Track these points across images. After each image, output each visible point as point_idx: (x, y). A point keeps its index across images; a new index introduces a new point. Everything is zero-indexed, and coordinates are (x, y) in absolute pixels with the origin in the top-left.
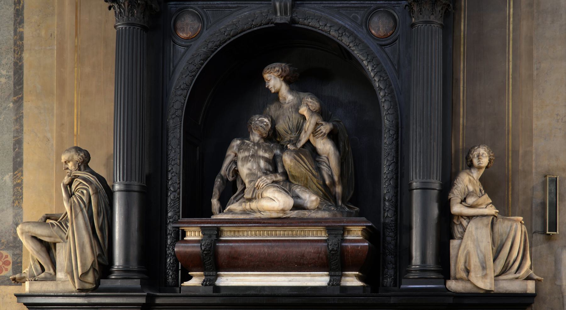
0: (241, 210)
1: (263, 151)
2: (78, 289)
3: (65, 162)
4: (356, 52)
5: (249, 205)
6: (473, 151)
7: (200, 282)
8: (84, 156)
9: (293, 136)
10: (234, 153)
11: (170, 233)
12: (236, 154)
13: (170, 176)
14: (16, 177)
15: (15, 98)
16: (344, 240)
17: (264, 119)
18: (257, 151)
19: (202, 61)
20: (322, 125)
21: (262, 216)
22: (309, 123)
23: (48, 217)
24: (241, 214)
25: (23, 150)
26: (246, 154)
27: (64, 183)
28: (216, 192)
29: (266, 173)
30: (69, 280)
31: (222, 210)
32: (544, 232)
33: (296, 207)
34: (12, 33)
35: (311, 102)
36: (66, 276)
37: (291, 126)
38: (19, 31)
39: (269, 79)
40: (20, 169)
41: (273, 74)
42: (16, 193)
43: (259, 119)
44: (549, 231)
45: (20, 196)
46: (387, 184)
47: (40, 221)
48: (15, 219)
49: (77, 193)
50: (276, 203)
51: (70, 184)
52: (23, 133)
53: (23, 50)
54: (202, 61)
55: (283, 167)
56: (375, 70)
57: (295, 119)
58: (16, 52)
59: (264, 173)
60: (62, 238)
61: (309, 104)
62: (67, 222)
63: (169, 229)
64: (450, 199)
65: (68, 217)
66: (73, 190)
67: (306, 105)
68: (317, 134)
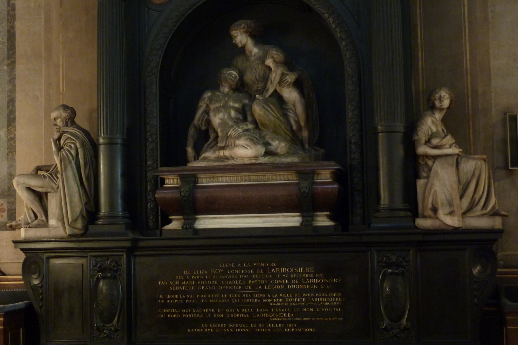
0: (215, 157)
1: (233, 101)
2: (68, 235)
3: (54, 119)
4: (317, 6)
5: (222, 153)
6: (434, 93)
7: (180, 225)
8: (71, 113)
9: (260, 86)
10: (206, 104)
11: (150, 180)
12: (207, 105)
13: (148, 128)
14: (10, 132)
15: (9, 62)
16: (314, 183)
17: (232, 71)
18: (227, 102)
19: (174, 24)
20: (287, 75)
21: (236, 163)
22: (275, 74)
23: (39, 168)
24: (216, 161)
25: (16, 108)
26: (218, 105)
27: (54, 138)
28: (190, 141)
29: (237, 122)
30: (60, 227)
31: (197, 157)
32: (506, 168)
33: (268, 153)
34: (6, 4)
35: (275, 54)
36: (57, 223)
37: (257, 77)
38: (12, 3)
39: (236, 36)
40: (13, 125)
41: (240, 31)
42: (10, 147)
43: (228, 72)
44: (512, 167)
45: (13, 149)
46: (352, 128)
47: (32, 173)
48: (9, 170)
49: (65, 147)
50: (248, 150)
51: (59, 139)
52: (15, 93)
53: (15, 19)
54: (174, 24)
55: (252, 115)
56: (336, 22)
57: (260, 70)
58: (9, 22)
59: (235, 122)
60: (52, 188)
61: (275, 56)
62: (57, 174)
63: (149, 176)
64: (415, 140)
65: (57, 168)
66: (62, 144)
67: (271, 57)
68: (283, 83)
